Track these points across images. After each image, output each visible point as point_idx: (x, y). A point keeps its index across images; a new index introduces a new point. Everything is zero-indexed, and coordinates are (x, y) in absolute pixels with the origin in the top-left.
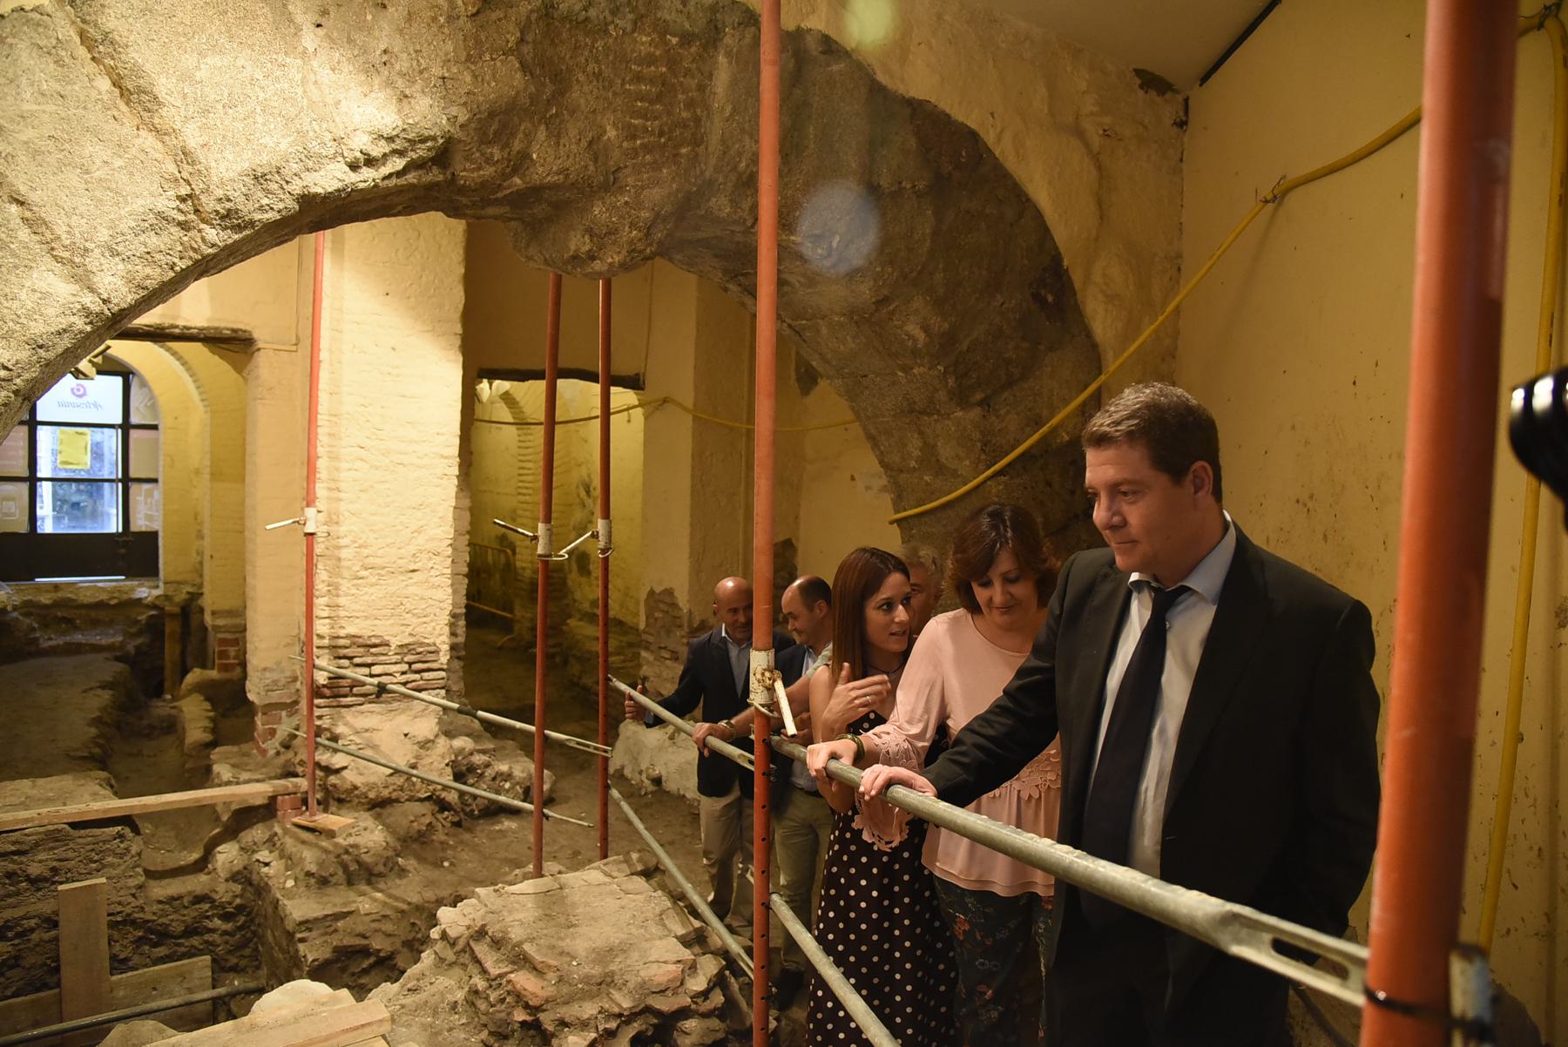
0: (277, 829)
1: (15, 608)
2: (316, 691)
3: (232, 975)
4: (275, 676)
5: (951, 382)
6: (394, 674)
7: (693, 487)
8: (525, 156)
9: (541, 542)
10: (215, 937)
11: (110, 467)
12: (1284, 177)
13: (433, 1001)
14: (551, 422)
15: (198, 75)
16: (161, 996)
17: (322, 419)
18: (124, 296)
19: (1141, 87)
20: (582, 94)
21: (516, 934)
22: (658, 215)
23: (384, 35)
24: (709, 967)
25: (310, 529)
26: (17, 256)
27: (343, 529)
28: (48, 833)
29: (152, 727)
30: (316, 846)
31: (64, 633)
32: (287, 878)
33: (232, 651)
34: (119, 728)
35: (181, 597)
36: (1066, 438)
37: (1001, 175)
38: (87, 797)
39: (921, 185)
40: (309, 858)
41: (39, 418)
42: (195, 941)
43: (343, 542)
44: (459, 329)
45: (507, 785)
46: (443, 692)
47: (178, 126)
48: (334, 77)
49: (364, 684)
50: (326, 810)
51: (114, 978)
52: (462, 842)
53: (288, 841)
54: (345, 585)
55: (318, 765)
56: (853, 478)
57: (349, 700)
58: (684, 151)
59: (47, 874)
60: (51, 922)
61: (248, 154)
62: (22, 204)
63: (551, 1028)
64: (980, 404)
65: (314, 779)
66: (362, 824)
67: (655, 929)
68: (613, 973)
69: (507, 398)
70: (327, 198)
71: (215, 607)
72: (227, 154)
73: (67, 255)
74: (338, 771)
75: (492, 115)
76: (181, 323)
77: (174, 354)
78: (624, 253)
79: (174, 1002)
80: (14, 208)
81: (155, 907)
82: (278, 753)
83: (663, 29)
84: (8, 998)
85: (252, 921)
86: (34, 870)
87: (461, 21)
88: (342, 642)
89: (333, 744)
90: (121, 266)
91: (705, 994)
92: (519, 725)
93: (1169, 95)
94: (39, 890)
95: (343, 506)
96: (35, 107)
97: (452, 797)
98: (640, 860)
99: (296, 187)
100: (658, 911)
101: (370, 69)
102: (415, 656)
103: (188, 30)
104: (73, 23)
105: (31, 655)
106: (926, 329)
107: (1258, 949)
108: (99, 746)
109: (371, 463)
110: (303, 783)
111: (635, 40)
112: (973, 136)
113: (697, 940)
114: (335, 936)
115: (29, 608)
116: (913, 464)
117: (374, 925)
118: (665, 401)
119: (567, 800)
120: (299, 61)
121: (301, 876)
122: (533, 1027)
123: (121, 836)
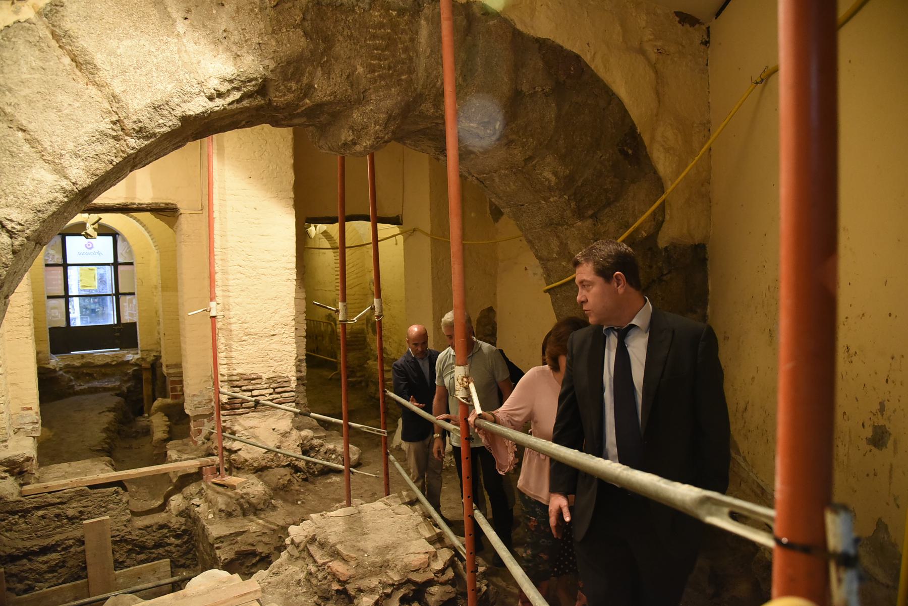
0: (203, 486)
1: (61, 369)
2: (222, 407)
3: (182, 569)
4: (200, 399)
5: (573, 205)
7: (433, 279)
8: (310, 86)
9: (341, 313)
10: (172, 548)
11: (109, 289)
12: (767, 67)
13: (286, 579)
14: (343, 247)
15: (119, 51)
16: (143, 582)
17: (217, 251)
18: (85, 180)
19: (679, 22)
20: (341, 48)
21: (332, 539)
22: (390, 116)
23: (223, 22)
24: (445, 555)
25: (213, 313)
26: (22, 160)
27: (232, 313)
28: (76, 492)
29: (137, 432)
30: (225, 494)
31: (88, 382)
32: (209, 513)
33: (178, 387)
34: (119, 433)
35: (151, 358)
36: (645, 234)
37: (596, 80)
38: (98, 471)
39: (547, 89)
41: (68, 262)
42: (161, 550)
43: (232, 320)
44: (292, 195)
45: (333, 456)
46: (294, 404)
47: (109, 81)
48: (196, 47)
49: (248, 402)
50: (230, 474)
51: (117, 572)
52: (308, 490)
53: (209, 492)
54: (235, 345)
55: (224, 448)
56: (526, 269)
57: (240, 411)
58: (403, 77)
59: (77, 515)
60: (81, 542)
61: (149, 95)
62: (24, 131)
63: (353, 593)
64: (591, 217)
65: (223, 457)
66: (251, 481)
67: (413, 534)
68: (388, 561)
69: (325, 234)
70: (197, 118)
71: (168, 363)
72: (137, 95)
73: (51, 158)
74: (236, 452)
75: (289, 63)
76: (137, 201)
77: (135, 218)
78: (372, 139)
79: (150, 585)
80: (20, 134)
81: (137, 532)
82: (203, 443)
83: (387, 8)
84: (60, 584)
85: (192, 538)
86: (71, 512)
87: (268, 11)
88: (235, 378)
89: (232, 436)
90: (82, 163)
91: (443, 571)
92: (334, 420)
93: (697, 26)
94: (73, 524)
95: (231, 300)
96: (30, 76)
97: (301, 464)
98: (408, 496)
99: (178, 112)
100: (415, 524)
101: (216, 42)
102: (277, 384)
103: (112, 26)
104: (48, 27)
105: (70, 395)
106: (555, 174)
107: (722, 518)
108: (106, 443)
109: (245, 272)
110: (217, 459)
111: (371, 14)
112: (578, 57)
113: (438, 540)
114: (236, 545)
115: (68, 368)
116: (555, 255)
117: (258, 538)
118: (414, 230)
119: (369, 464)
120: (176, 40)
121: (217, 512)
122: (343, 593)
123: (117, 492)
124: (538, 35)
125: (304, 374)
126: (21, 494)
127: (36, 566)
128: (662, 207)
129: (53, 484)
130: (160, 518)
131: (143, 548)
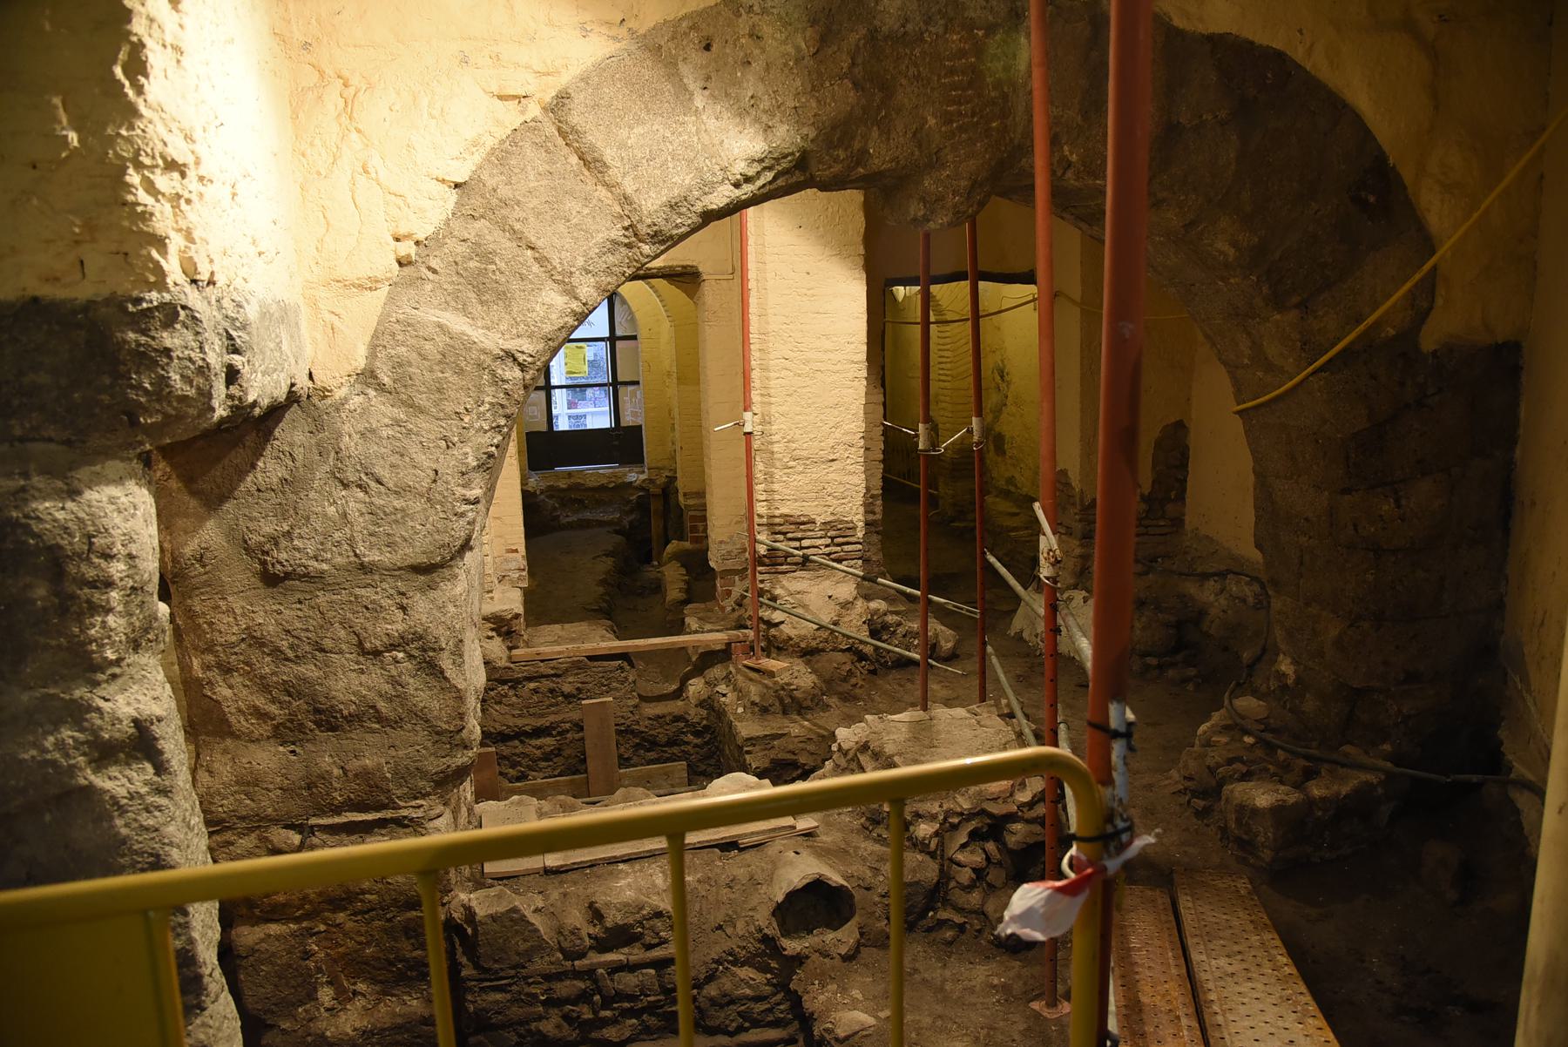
2: (758, 561)
4: (729, 548)
5: (1265, 289)
6: (817, 545)
8: (864, 151)
17: (754, 337)
23: (751, 85)
25: (748, 429)
35: (661, 481)
36: (1392, 332)
40: (754, 692)
42: (675, 750)
50: (768, 656)
54: (778, 474)
55: (761, 619)
64: (1297, 306)
74: (777, 625)
75: (833, 128)
80: (529, 252)
83: (970, 26)
86: (567, 688)
88: (777, 520)
91: (1031, 805)
95: (773, 409)
97: (868, 650)
99: (699, 207)
101: (741, 113)
102: (837, 531)
106: (1234, 244)
110: (751, 634)
112: (1280, 56)
124: (1211, 31)
125: (879, 517)
126: (510, 658)
127: (529, 750)
128: (1429, 286)
129: (546, 650)
130: (675, 707)
131: (653, 744)
